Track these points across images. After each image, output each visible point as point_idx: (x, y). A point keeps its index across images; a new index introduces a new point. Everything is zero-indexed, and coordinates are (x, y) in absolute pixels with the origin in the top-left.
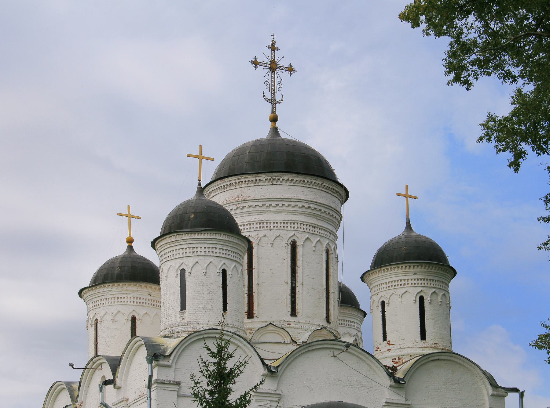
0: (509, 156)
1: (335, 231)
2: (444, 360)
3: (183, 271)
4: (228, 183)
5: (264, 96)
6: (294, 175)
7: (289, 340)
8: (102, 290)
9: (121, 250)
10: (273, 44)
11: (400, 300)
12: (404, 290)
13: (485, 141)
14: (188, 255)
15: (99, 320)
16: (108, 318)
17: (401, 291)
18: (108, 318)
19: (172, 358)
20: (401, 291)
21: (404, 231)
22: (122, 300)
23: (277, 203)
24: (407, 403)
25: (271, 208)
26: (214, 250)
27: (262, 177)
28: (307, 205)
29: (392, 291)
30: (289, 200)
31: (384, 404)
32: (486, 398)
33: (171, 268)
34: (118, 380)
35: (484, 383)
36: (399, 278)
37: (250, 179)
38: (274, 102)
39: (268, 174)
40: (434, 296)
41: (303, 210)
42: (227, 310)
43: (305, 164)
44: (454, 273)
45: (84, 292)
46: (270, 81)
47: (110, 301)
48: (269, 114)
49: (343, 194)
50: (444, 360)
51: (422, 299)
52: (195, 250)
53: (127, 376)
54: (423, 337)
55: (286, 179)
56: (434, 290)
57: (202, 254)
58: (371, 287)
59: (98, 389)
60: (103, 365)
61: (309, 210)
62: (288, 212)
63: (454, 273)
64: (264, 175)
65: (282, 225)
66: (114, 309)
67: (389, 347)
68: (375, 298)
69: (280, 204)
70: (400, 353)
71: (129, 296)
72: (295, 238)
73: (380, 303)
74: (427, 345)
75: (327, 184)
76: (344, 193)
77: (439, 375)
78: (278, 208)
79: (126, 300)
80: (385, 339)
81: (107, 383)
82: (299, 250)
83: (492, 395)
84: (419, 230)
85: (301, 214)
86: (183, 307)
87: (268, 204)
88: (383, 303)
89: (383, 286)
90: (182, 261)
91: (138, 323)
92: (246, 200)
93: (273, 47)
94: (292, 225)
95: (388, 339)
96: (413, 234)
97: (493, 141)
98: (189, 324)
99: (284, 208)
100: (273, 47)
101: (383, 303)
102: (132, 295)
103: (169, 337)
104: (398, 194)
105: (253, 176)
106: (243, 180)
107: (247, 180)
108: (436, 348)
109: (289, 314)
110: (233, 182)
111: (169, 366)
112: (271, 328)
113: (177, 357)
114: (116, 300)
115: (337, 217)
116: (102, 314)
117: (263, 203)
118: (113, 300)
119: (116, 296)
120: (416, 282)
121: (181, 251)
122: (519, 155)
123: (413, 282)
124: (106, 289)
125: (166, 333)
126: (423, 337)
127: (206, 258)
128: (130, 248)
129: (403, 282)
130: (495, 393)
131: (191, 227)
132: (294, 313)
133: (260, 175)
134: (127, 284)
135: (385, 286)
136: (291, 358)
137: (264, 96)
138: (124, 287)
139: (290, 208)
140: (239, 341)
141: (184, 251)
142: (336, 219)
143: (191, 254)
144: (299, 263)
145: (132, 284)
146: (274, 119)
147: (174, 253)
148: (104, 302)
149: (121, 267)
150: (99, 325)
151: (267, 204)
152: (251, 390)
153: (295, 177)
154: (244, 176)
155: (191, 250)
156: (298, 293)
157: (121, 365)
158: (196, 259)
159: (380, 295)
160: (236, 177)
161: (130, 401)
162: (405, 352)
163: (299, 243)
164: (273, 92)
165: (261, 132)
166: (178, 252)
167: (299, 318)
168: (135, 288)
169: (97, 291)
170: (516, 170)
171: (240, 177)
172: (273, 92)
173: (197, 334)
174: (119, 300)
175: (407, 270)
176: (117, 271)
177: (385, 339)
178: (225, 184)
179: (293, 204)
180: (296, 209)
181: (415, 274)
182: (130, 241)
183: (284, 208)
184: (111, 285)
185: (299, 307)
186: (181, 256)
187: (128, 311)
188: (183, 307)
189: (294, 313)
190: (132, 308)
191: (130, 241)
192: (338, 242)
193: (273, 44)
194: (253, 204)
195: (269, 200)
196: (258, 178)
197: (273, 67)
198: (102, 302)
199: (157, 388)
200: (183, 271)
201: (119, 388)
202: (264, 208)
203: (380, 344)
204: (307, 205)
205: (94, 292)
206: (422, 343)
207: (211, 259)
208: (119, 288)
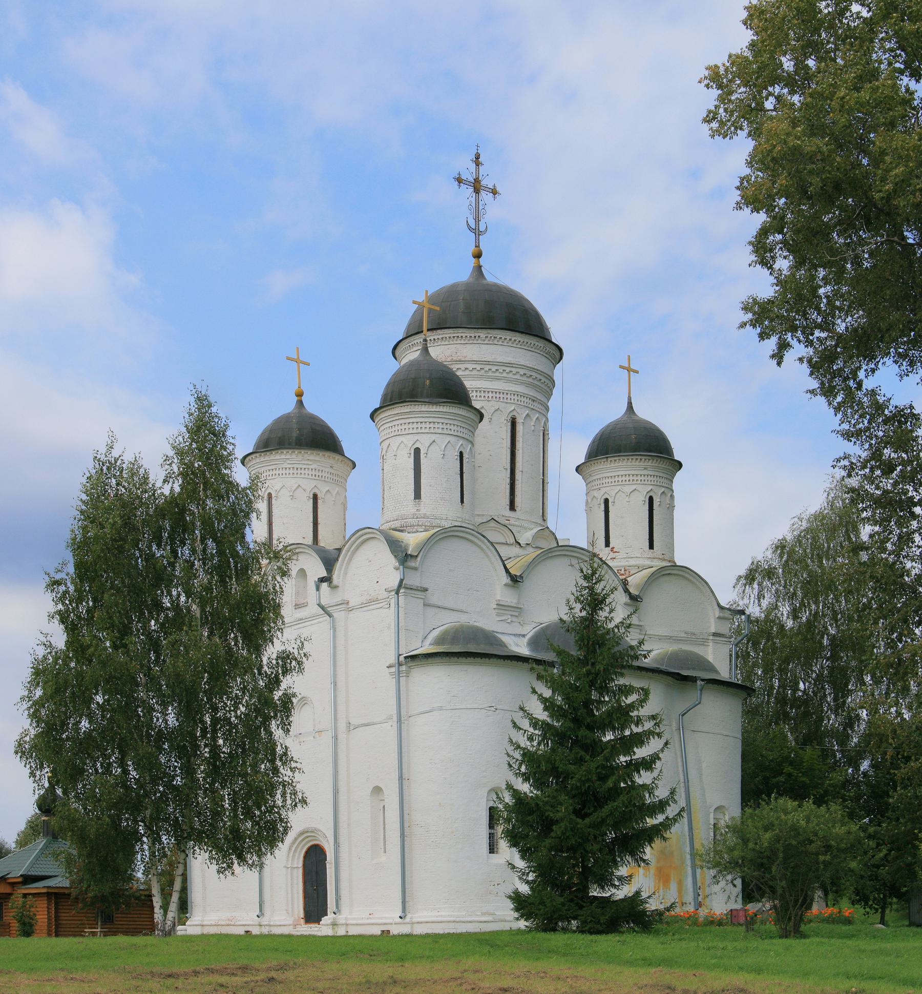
0: (772, 343)
1: (545, 401)
2: (675, 575)
3: (417, 451)
4: (440, 337)
5: (468, 225)
6: (517, 334)
7: (512, 540)
8: (278, 457)
9: (288, 406)
10: (477, 157)
11: (627, 499)
12: (634, 487)
13: (703, 84)
14: (423, 431)
15: (273, 495)
16: (285, 494)
17: (628, 489)
18: (285, 494)
19: (419, 559)
20: (628, 489)
21: (626, 413)
22: (303, 471)
23: (496, 368)
24: (641, 624)
25: (490, 374)
26: (452, 427)
27: (482, 334)
28: (529, 373)
29: (619, 488)
30: (509, 364)
31: (495, 606)
32: (712, 620)
33: (402, 445)
34: (335, 577)
35: (299, 858)
36: (627, 473)
37: (468, 335)
38: (477, 233)
39: (489, 331)
40: (663, 496)
41: (525, 378)
42: (105, 936)
43: (515, 318)
44: (679, 465)
45: (247, 459)
46: (474, 205)
47: (288, 471)
48: (472, 248)
49: (557, 354)
50: (675, 575)
51: (651, 500)
52: (432, 425)
53: (345, 574)
54: (651, 546)
55: (508, 338)
56: (663, 489)
57: (440, 431)
58: (591, 479)
59: (314, 588)
60: (323, 603)
61: (530, 380)
62: (508, 381)
63: (679, 465)
64: (485, 331)
65: (501, 396)
66: (292, 483)
67: (612, 555)
68: (595, 493)
69: (501, 369)
70: (627, 563)
71: (311, 467)
72: (514, 413)
73: (602, 501)
74: (655, 555)
75: (541, 343)
76: (558, 351)
77: (669, 590)
78: (497, 374)
79: (307, 472)
80: (607, 544)
81: (322, 580)
82: (520, 428)
83: (719, 618)
84: (312, 407)
85: (522, 383)
86: (418, 495)
87: (487, 368)
88: (606, 501)
89: (607, 480)
90: (416, 437)
91: (320, 502)
92: (452, 351)
93: (477, 160)
94: (513, 397)
95: (611, 545)
96: (484, 282)
97: (283, 686)
98: (425, 516)
99: (505, 375)
100: (477, 160)
101: (606, 501)
102: (313, 467)
103: (402, 531)
104: (637, 372)
105: (473, 331)
106: (460, 335)
107: (464, 335)
108: (664, 560)
109: (508, 507)
110: (447, 336)
111: (416, 569)
112: (493, 524)
113: (293, 849)
114: (295, 471)
115: (550, 384)
116: (278, 487)
117: (482, 366)
118: (291, 471)
119: (295, 466)
120: (646, 478)
121: (415, 426)
122: (783, 346)
123: (643, 478)
124: (283, 457)
125: (397, 524)
126: (651, 546)
127: (444, 436)
128: (300, 403)
129: (631, 478)
130: (721, 615)
131: (428, 397)
132: (512, 507)
133: (480, 331)
134: (309, 452)
135: (610, 480)
136: (533, 564)
137: (468, 225)
138: (306, 455)
139: (510, 375)
140: (483, 542)
141: (419, 425)
142: (546, 385)
143: (427, 430)
144: (519, 445)
145: (315, 452)
146: (478, 255)
147: (406, 426)
148: (281, 472)
149: (299, 429)
150: (274, 501)
151: (487, 367)
152: (830, 404)
153: (518, 337)
154: (461, 330)
155: (428, 425)
156: (517, 482)
157: (340, 559)
158: (434, 437)
159: (603, 490)
160: (451, 331)
161: (351, 605)
162: (632, 562)
163: (519, 420)
164: (477, 220)
165: (462, 274)
166: (411, 426)
167: (518, 513)
168: (317, 458)
169: (272, 457)
170: (779, 364)
171: (456, 330)
172: (477, 220)
173: (370, 530)
174: (299, 471)
175: (637, 463)
176: (295, 434)
177: (607, 544)
178: (436, 337)
179: (514, 370)
180: (517, 377)
181: (645, 469)
182: (300, 395)
183: (505, 375)
184: (290, 451)
185: (518, 500)
186: (415, 431)
187: (309, 486)
188: (418, 495)
189: (512, 507)
190: (314, 483)
191: (300, 395)
192: (550, 415)
193: (477, 157)
194: (470, 366)
195: (488, 363)
196: (477, 335)
197: (477, 186)
198: (277, 472)
199: (406, 595)
200: (417, 451)
201: (336, 587)
202: (482, 372)
203: (601, 550)
204: (529, 373)
205: (267, 458)
206: (650, 553)
207: (448, 438)
208: (300, 457)
